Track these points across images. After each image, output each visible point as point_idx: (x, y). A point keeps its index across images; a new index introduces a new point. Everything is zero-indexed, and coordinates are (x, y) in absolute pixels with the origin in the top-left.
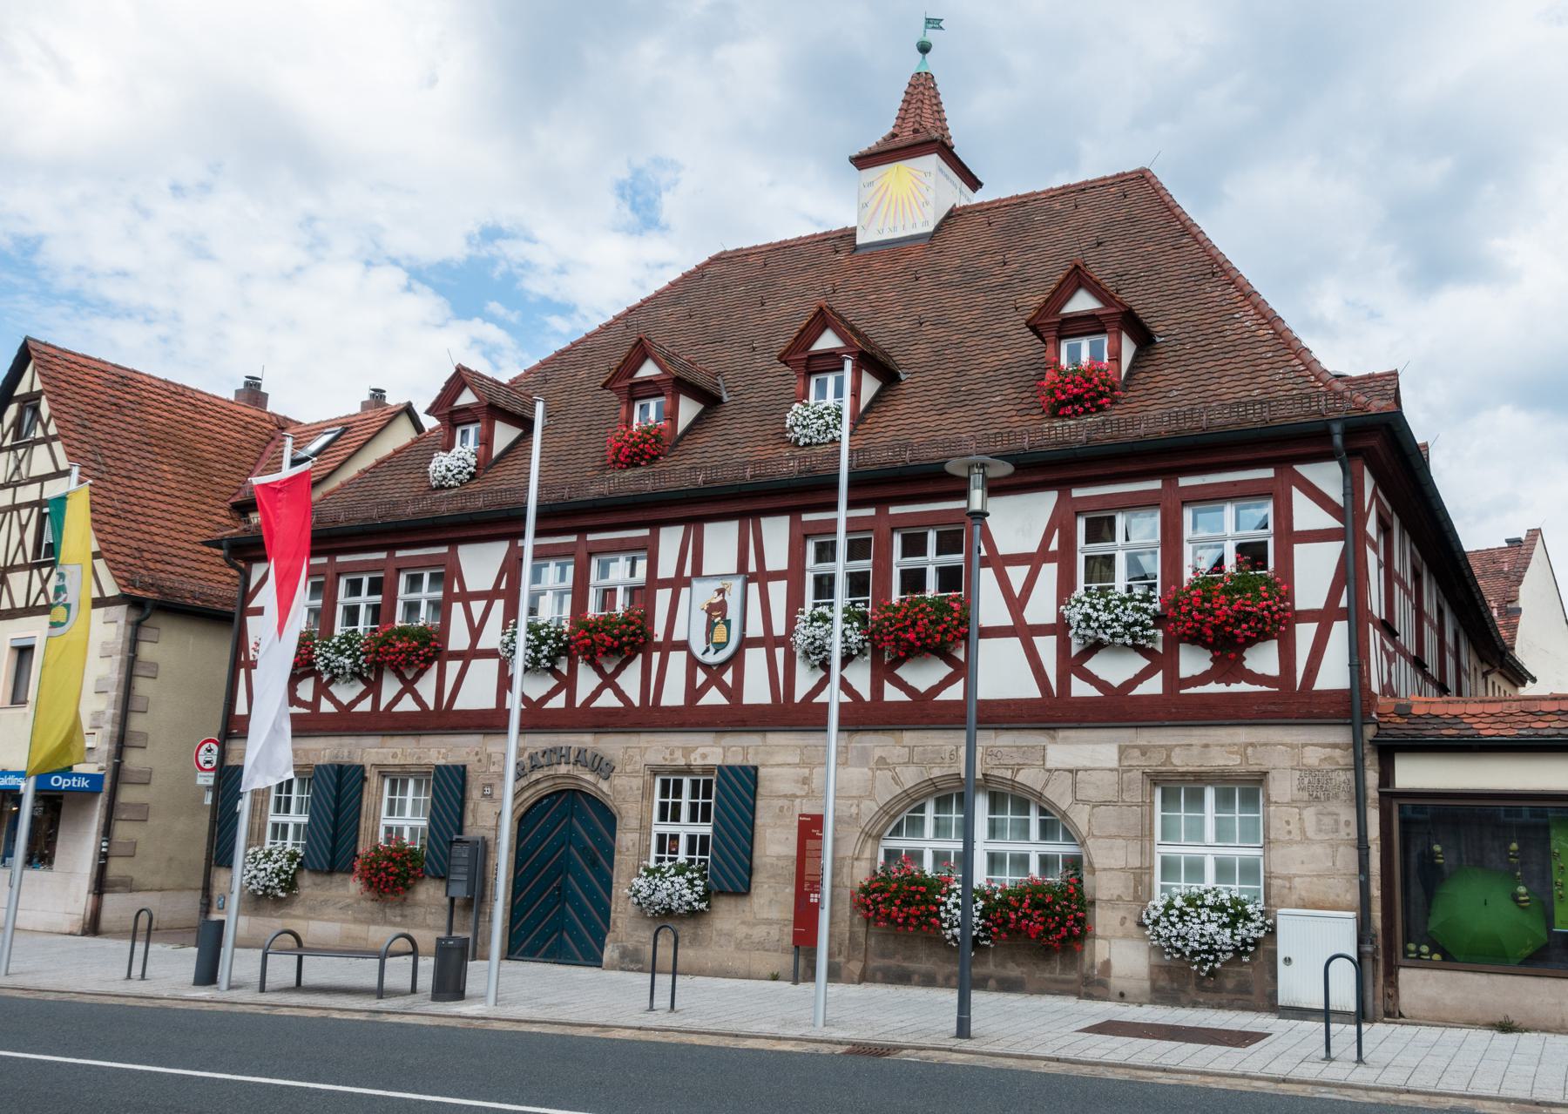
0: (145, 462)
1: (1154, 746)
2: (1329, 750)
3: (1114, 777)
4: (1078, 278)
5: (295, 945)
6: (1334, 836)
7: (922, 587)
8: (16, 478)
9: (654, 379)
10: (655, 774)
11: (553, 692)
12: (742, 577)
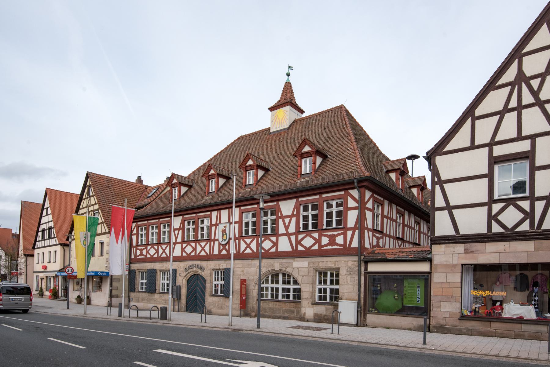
0: (114, 200)
1: (316, 262)
2: (353, 262)
4: (305, 142)
5: (136, 308)
6: (354, 283)
8: (88, 205)
9: (213, 174)
10: (213, 270)
11: (192, 252)
12: (229, 223)
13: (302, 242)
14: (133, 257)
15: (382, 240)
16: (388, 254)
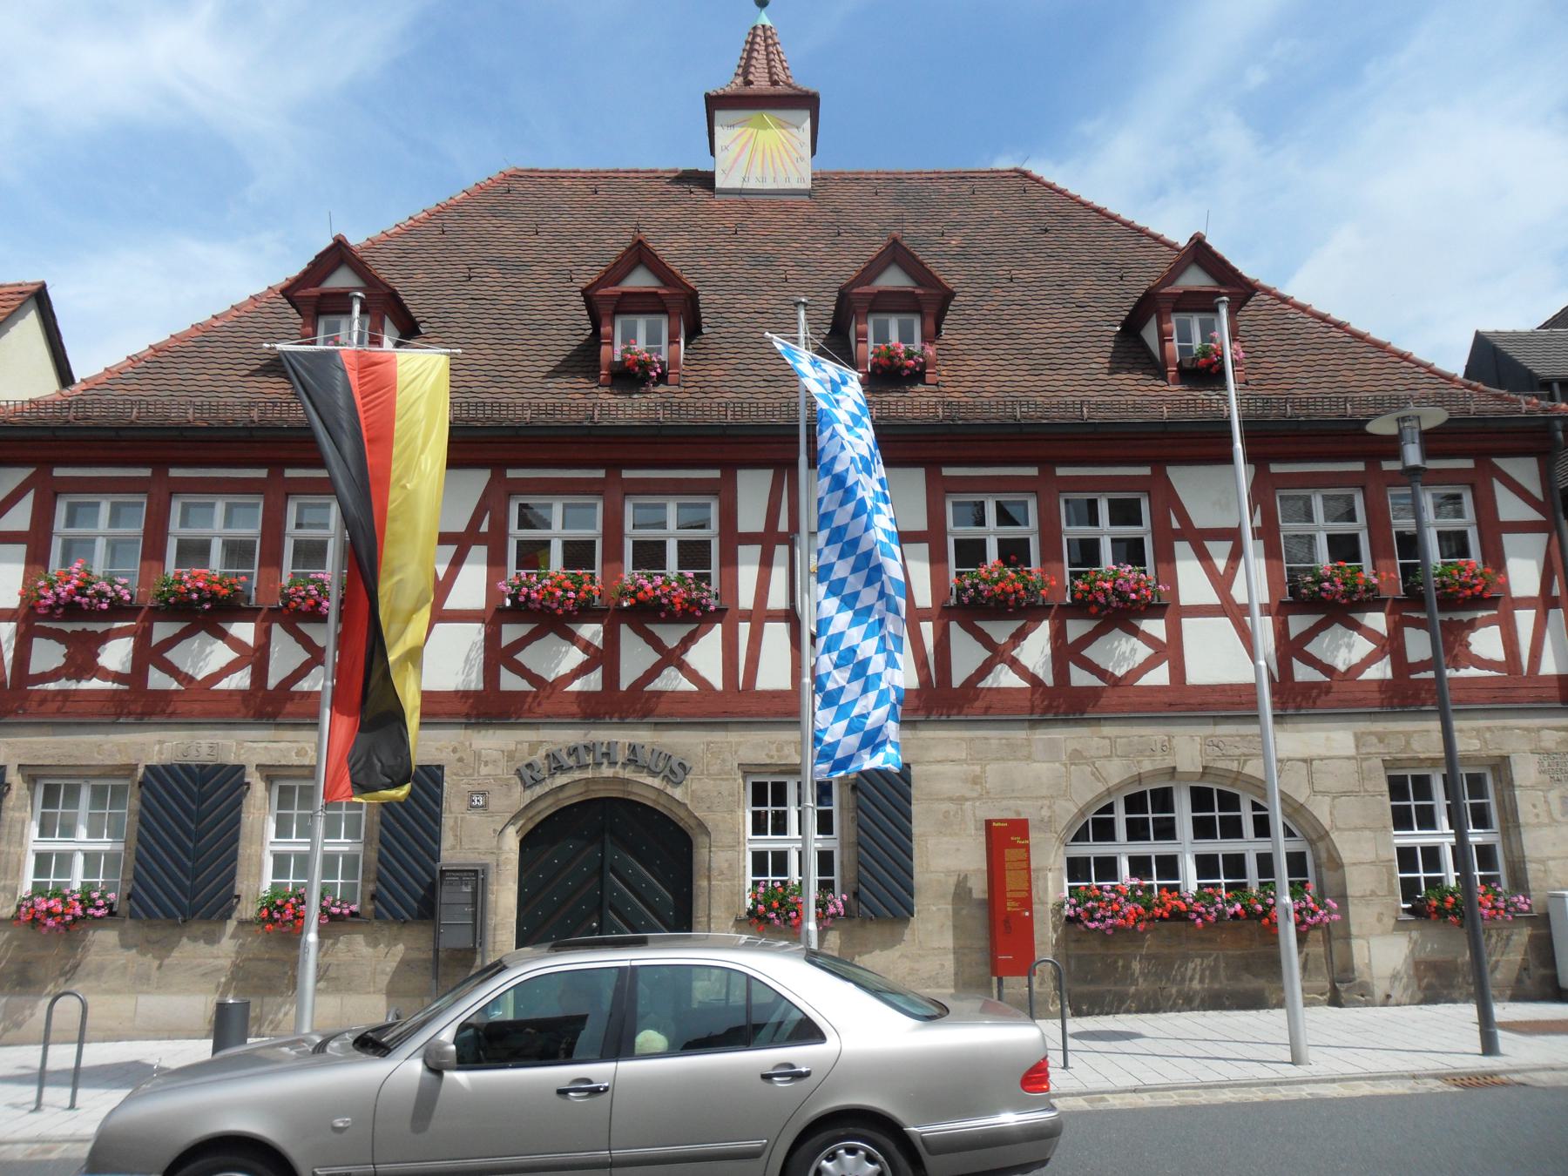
3: (1353, 765)
7: (660, 562)
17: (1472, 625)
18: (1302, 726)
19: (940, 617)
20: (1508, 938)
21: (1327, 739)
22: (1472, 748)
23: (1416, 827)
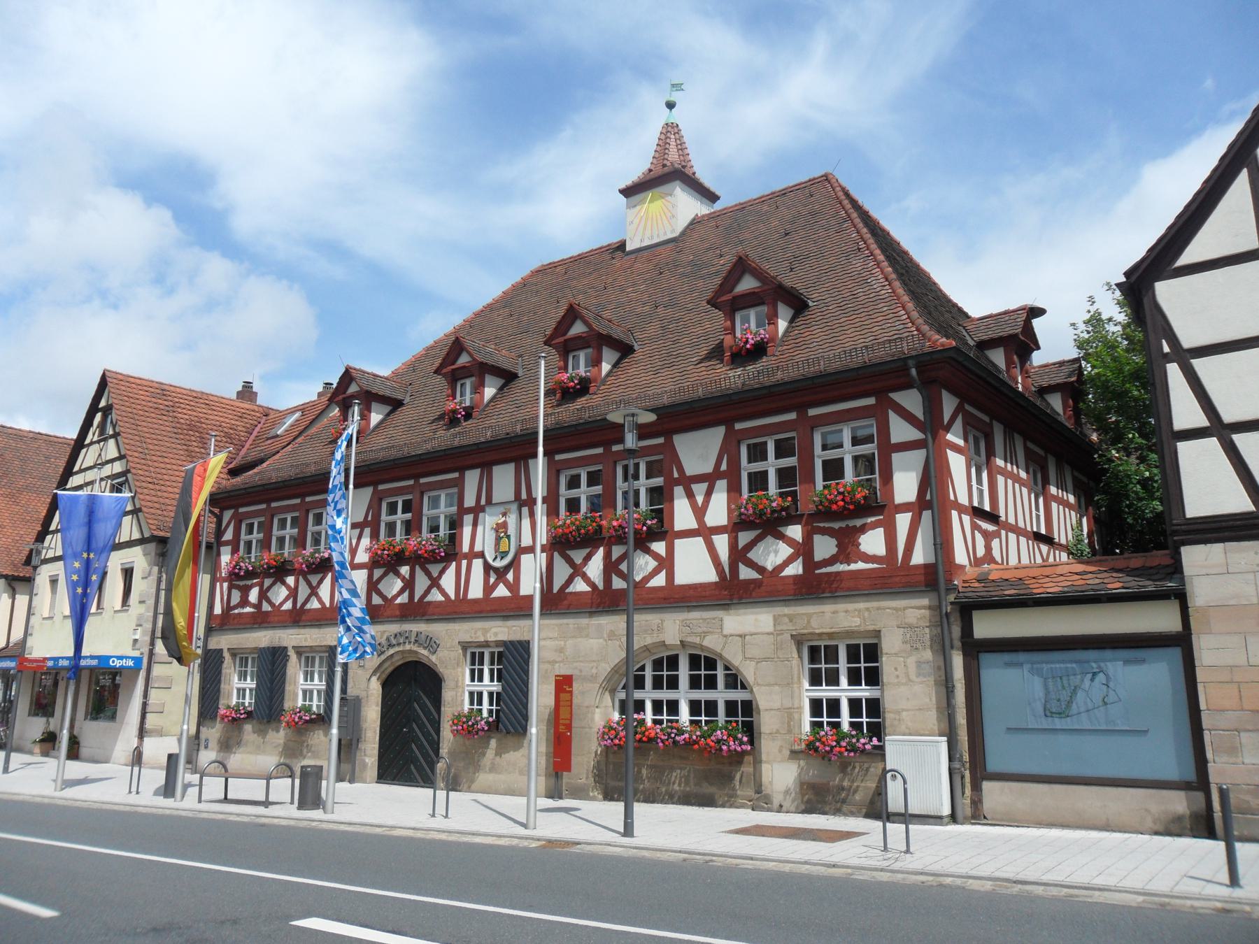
11: (655, 572)
13: (751, 555)
14: (218, 610)
15: (998, 540)
16: (1034, 581)
17: (863, 529)
18: (742, 611)
19: (550, 550)
20: (867, 770)
21: (756, 620)
22: (853, 625)
23: (824, 684)
